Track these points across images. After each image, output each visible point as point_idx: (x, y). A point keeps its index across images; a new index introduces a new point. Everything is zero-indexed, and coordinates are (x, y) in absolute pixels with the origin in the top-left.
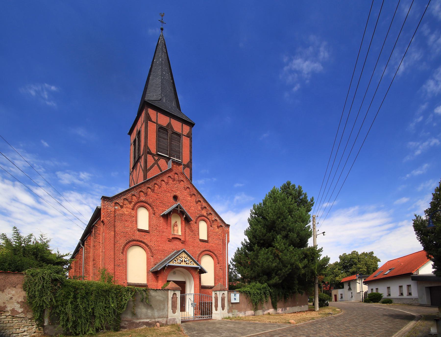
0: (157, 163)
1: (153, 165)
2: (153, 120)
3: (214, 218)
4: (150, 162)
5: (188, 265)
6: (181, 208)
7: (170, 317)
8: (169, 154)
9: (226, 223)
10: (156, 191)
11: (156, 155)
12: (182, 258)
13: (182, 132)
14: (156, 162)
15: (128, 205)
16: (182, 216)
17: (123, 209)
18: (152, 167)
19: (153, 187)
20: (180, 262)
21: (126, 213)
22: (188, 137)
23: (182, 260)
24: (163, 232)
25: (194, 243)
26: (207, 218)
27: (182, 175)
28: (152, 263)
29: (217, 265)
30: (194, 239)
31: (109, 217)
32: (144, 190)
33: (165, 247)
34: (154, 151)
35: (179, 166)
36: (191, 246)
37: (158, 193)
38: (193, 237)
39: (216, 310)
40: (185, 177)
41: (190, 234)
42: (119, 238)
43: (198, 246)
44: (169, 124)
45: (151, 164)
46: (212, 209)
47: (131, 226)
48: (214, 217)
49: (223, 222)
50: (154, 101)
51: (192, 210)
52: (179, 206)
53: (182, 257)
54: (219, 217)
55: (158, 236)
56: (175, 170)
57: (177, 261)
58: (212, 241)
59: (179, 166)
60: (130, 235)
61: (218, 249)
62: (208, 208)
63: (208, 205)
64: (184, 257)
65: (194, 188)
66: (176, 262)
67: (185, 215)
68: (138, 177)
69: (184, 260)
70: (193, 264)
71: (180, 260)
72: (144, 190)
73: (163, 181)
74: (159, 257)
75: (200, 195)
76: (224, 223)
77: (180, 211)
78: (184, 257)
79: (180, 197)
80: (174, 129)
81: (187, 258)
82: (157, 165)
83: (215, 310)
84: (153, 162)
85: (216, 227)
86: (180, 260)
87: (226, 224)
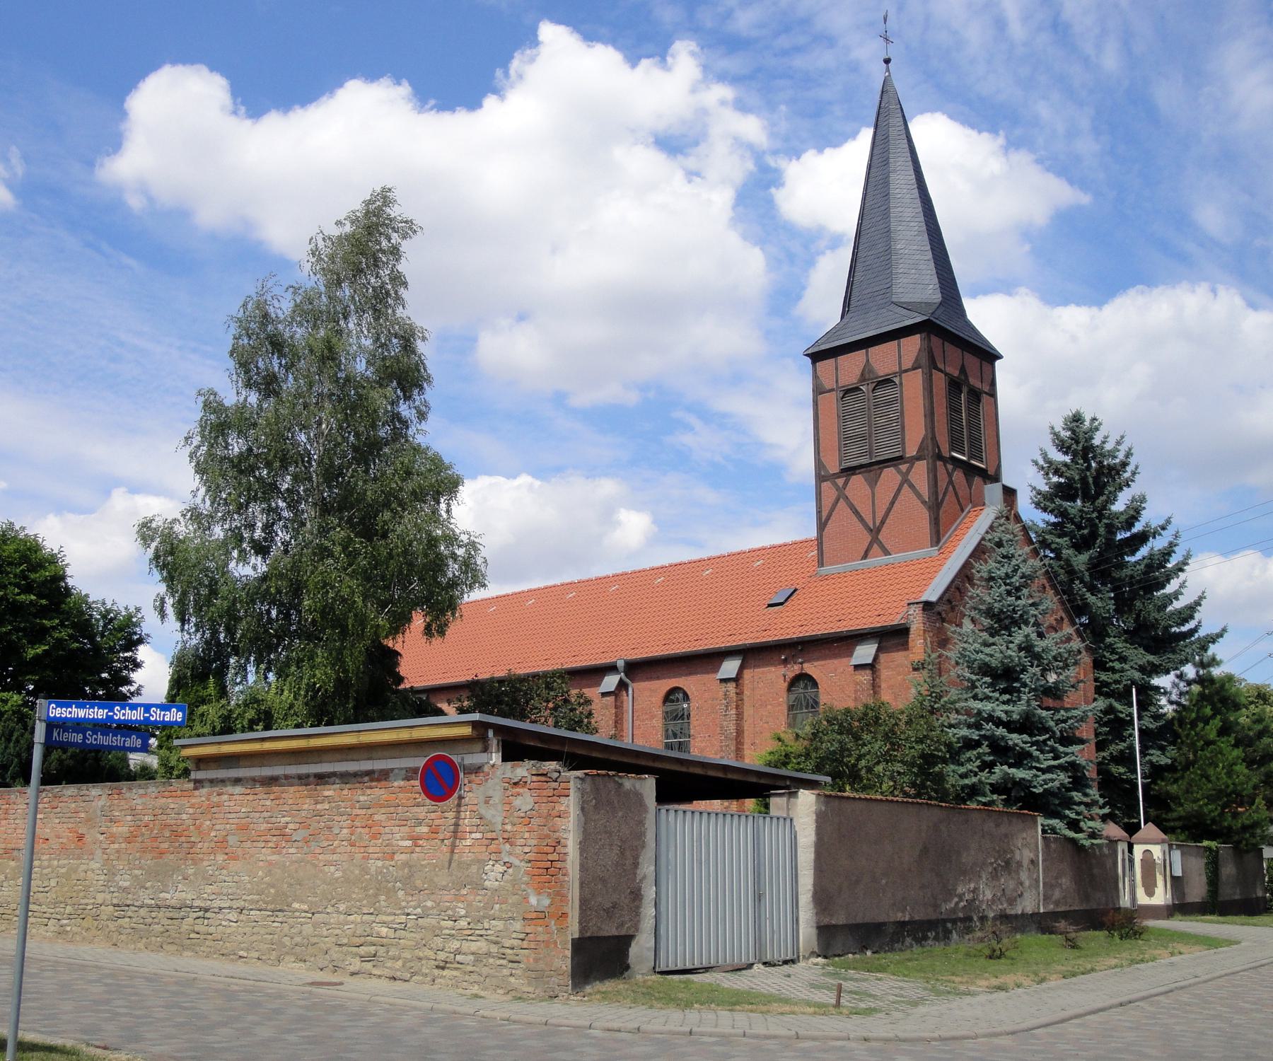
18: (945, 494)
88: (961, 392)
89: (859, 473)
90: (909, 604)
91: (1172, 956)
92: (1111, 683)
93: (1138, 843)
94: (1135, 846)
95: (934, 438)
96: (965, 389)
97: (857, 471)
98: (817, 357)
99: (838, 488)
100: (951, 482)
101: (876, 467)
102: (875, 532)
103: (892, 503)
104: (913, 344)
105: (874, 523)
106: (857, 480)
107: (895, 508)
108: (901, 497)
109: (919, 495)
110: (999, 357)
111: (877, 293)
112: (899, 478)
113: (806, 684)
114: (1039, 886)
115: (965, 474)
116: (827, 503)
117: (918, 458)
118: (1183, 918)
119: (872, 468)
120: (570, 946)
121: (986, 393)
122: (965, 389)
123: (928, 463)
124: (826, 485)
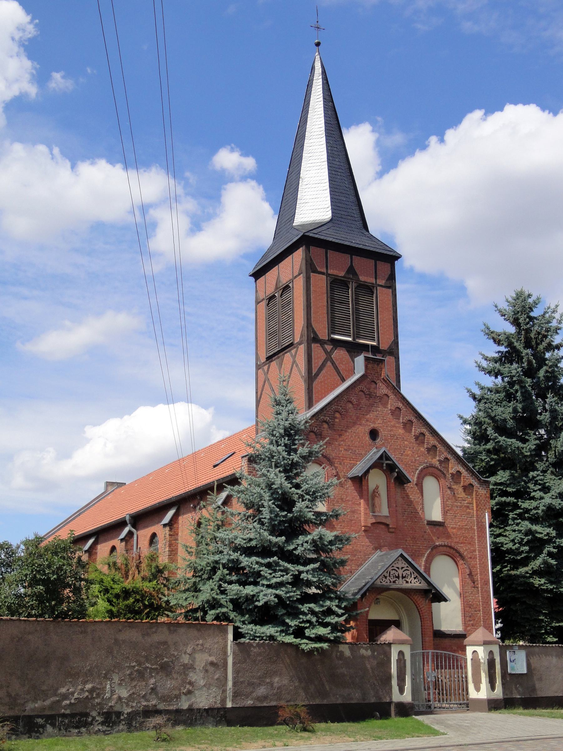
0: (331, 358)
5: (409, 586)
6: (388, 458)
8: (352, 334)
11: (329, 343)
12: (397, 571)
14: (329, 357)
16: (389, 473)
19: (331, 419)
20: (395, 579)
23: (397, 576)
25: (415, 531)
30: (415, 522)
32: (316, 429)
34: (323, 334)
35: (378, 365)
36: (410, 539)
37: (342, 430)
38: (412, 517)
41: (405, 511)
43: (423, 536)
45: (320, 363)
50: (319, 230)
51: (408, 455)
52: (384, 455)
53: (398, 568)
54: (464, 464)
56: (372, 374)
57: (388, 578)
58: (451, 522)
59: (378, 365)
61: (466, 540)
64: (402, 568)
66: (387, 580)
67: (397, 472)
69: (402, 574)
70: (420, 581)
71: (394, 575)
72: (316, 429)
73: (351, 402)
75: (422, 420)
77: (386, 464)
78: (402, 568)
79: (383, 433)
81: (408, 570)
82: (331, 362)
83: (385, 721)
84: (323, 356)
86: (394, 575)
88: (349, 288)
89: (274, 360)
90: (242, 457)
91: (265, 746)
92: (531, 510)
93: (469, 645)
94: (467, 647)
96: (352, 286)
97: (274, 358)
98: (257, 275)
101: (281, 354)
104: (299, 255)
106: (274, 364)
108: (292, 375)
114: (225, 684)
115: (348, 351)
118: (526, 711)
119: (279, 355)
120: (229, 728)
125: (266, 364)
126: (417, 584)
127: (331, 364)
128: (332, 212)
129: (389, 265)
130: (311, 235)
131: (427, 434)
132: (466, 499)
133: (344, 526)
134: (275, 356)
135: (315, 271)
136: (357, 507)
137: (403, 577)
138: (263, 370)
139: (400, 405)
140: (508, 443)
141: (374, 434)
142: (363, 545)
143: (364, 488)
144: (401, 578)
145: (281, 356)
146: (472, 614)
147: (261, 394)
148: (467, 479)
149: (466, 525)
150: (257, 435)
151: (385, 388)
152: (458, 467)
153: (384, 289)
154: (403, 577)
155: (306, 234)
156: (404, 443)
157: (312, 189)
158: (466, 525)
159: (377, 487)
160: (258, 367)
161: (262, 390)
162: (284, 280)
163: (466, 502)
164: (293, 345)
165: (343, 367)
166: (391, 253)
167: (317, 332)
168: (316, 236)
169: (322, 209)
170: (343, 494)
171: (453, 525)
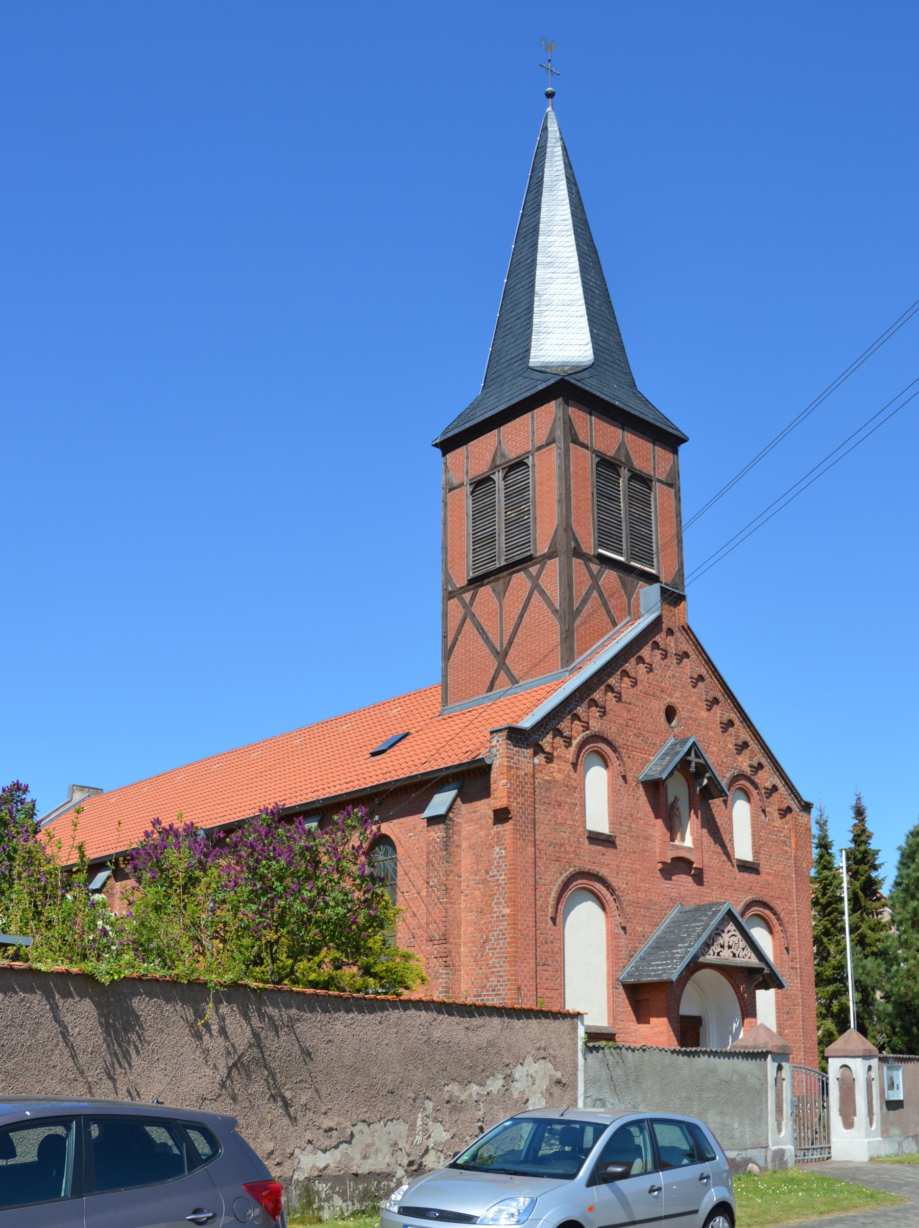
1: (587, 593)
2: (581, 438)
3: (769, 782)
4: (581, 582)
7: (773, 1145)
9: (801, 799)
10: (624, 698)
11: (595, 560)
13: (654, 469)
15: (562, 750)
17: (550, 765)
18: (584, 601)
21: (558, 776)
22: (671, 485)
24: (647, 838)
25: (723, 876)
26: (753, 783)
27: (685, 635)
28: (624, 953)
29: (784, 956)
31: (523, 796)
33: (652, 892)
34: (589, 545)
39: (848, 1124)
40: (691, 640)
42: (545, 866)
44: (622, 445)
46: (764, 749)
47: (571, 823)
48: (767, 778)
49: (794, 794)
55: (634, 853)
58: (766, 865)
60: (568, 853)
62: (753, 745)
63: (753, 733)
65: (716, 678)
67: (708, 778)
68: (518, 625)
74: (640, 929)
76: (797, 799)
77: (696, 763)
80: (635, 464)
85: (776, 815)
87: (805, 802)
89: (487, 584)
90: (492, 733)
95: (568, 528)
96: (625, 473)
97: (485, 581)
98: (447, 445)
99: (465, 606)
100: (595, 586)
101: (505, 573)
102: (502, 655)
103: (521, 616)
104: (551, 411)
105: (501, 643)
106: (486, 592)
107: (523, 623)
108: (531, 608)
109: (550, 603)
110: (683, 440)
111: (515, 360)
112: (529, 584)
113: (386, 849)
116: (453, 624)
117: (551, 555)
119: (501, 575)
121: (660, 481)
122: (625, 473)
123: (560, 561)
124: (454, 602)
125: (468, 591)
126: (746, 959)
127: (597, 595)
128: (594, 354)
129: (671, 455)
130: (573, 381)
131: (737, 722)
132: (783, 830)
133: (635, 861)
134: (489, 577)
135: (576, 441)
136: (651, 831)
137: (730, 947)
138: (462, 601)
139: (704, 672)
140: (572, 782)
141: (670, 713)
142: (659, 894)
143: (662, 799)
144: (726, 948)
145: (504, 577)
146: (790, 1009)
147: (456, 640)
148: (785, 798)
149: (783, 871)
150: (445, 708)
151: (685, 641)
152: (774, 778)
153: (664, 486)
154: (730, 947)
155: (567, 378)
156: (708, 733)
157: (558, 313)
158: (783, 871)
159: (676, 799)
160: (450, 595)
161: (459, 632)
162: (512, 453)
163: (782, 835)
164: (534, 559)
165: (614, 602)
166: (676, 433)
167: (579, 540)
168: (579, 384)
169: (577, 346)
170: (632, 808)
171: (768, 869)
